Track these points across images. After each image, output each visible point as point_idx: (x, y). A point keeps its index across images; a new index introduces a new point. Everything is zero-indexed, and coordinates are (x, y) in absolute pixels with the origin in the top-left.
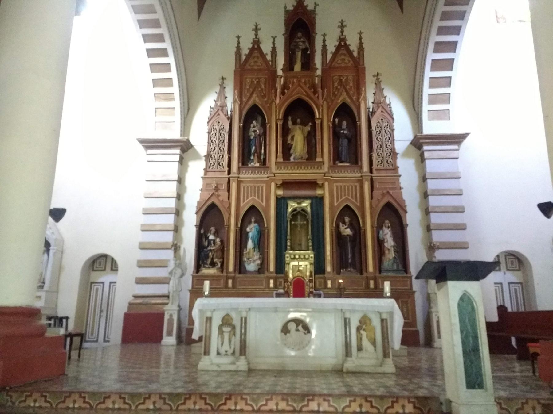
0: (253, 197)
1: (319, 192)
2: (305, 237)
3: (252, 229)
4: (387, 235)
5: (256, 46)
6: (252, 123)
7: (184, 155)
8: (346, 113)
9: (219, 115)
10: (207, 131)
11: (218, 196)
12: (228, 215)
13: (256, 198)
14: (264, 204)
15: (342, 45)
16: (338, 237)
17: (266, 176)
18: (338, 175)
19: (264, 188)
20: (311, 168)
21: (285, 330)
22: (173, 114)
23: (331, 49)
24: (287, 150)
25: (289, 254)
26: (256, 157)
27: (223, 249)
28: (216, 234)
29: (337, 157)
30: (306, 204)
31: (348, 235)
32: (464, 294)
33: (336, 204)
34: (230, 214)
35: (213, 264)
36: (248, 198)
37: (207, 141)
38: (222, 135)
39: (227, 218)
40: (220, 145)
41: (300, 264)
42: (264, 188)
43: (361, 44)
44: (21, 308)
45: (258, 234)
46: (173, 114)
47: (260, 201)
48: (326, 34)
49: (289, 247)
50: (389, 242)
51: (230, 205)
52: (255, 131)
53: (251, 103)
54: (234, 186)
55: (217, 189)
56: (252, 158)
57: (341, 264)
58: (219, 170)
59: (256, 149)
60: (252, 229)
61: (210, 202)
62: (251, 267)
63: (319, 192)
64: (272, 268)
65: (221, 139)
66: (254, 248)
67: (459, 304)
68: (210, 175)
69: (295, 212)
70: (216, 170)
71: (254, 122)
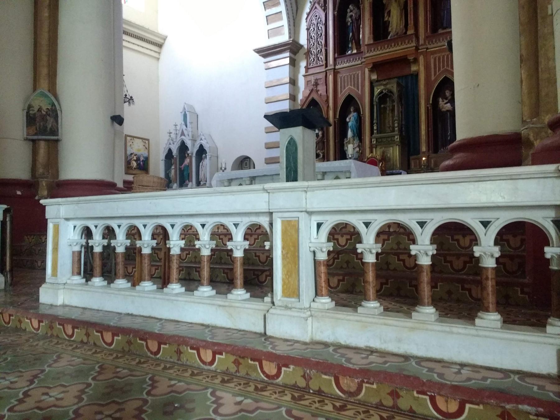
0: (349, 86)
3: (350, 118)
6: (348, 8)
7: (296, 57)
9: (316, 8)
10: (306, 27)
11: (317, 91)
12: (326, 108)
13: (352, 87)
14: (360, 92)
17: (359, 62)
19: (360, 75)
20: (401, 44)
22: (281, 19)
26: (354, 44)
31: (448, 111)
32: (292, 139)
33: (433, 78)
34: (328, 107)
36: (344, 88)
37: (306, 38)
38: (320, 28)
39: (326, 111)
40: (318, 40)
42: (360, 75)
44: (95, 180)
45: (357, 123)
46: (281, 19)
47: (356, 89)
49: (375, 131)
51: (328, 97)
52: (351, 16)
55: (316, 84)
56: (350, 46)
58: (318, 65)
59: (353, 35)
60: (351, 119)
61: (310, 98)
65: (319, 33)
66: (353, 137)
67: (287, 147)
69: (381, 95)
70: (316, 65)
71: (350, 6)
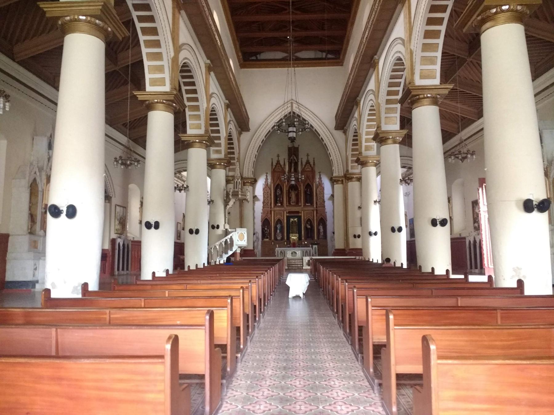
1: (300, 214)
2: (295, 229)
4: (321, 228)
5: (278, 162)
8: (309, 187)
15: (308, 162)
16: (306, 228)
18: (306, 208)
21: (292, 253)
23: (304, 163)
24: (289, 198)
25: (291, 235)
27: (270, 234)
28: (268, 228)
29: (306, 201)
30: (296, 219)
35: (267, 238)
41: (294, 237)
43: (314, 162)
48: (303, 157)
50: (322, 230)
53: (277, 183)
54: (273, 212)
57: (307, 237)
60: (279, 226)
62: (279, 238)
63: (300, 214)
64: (286, 238)
68: (265, 209)
